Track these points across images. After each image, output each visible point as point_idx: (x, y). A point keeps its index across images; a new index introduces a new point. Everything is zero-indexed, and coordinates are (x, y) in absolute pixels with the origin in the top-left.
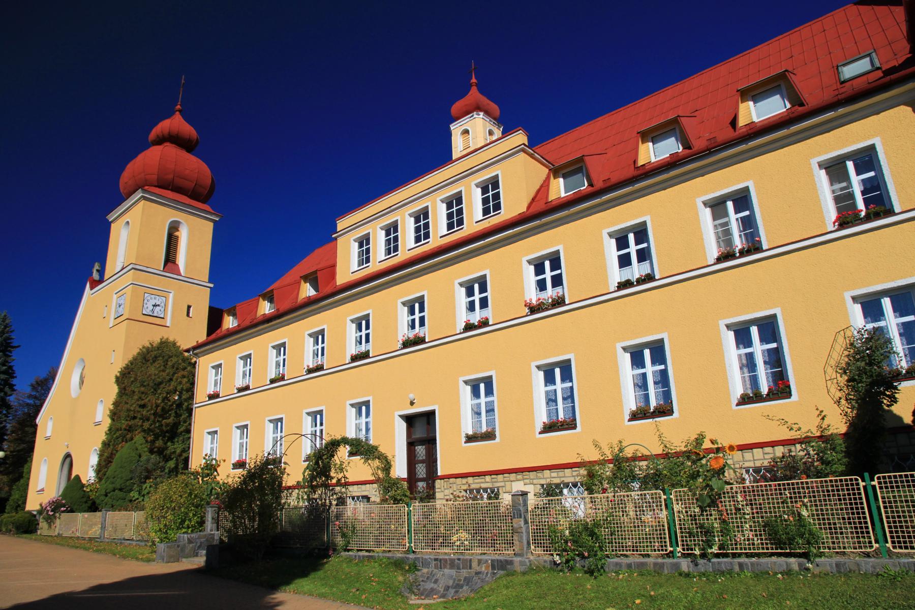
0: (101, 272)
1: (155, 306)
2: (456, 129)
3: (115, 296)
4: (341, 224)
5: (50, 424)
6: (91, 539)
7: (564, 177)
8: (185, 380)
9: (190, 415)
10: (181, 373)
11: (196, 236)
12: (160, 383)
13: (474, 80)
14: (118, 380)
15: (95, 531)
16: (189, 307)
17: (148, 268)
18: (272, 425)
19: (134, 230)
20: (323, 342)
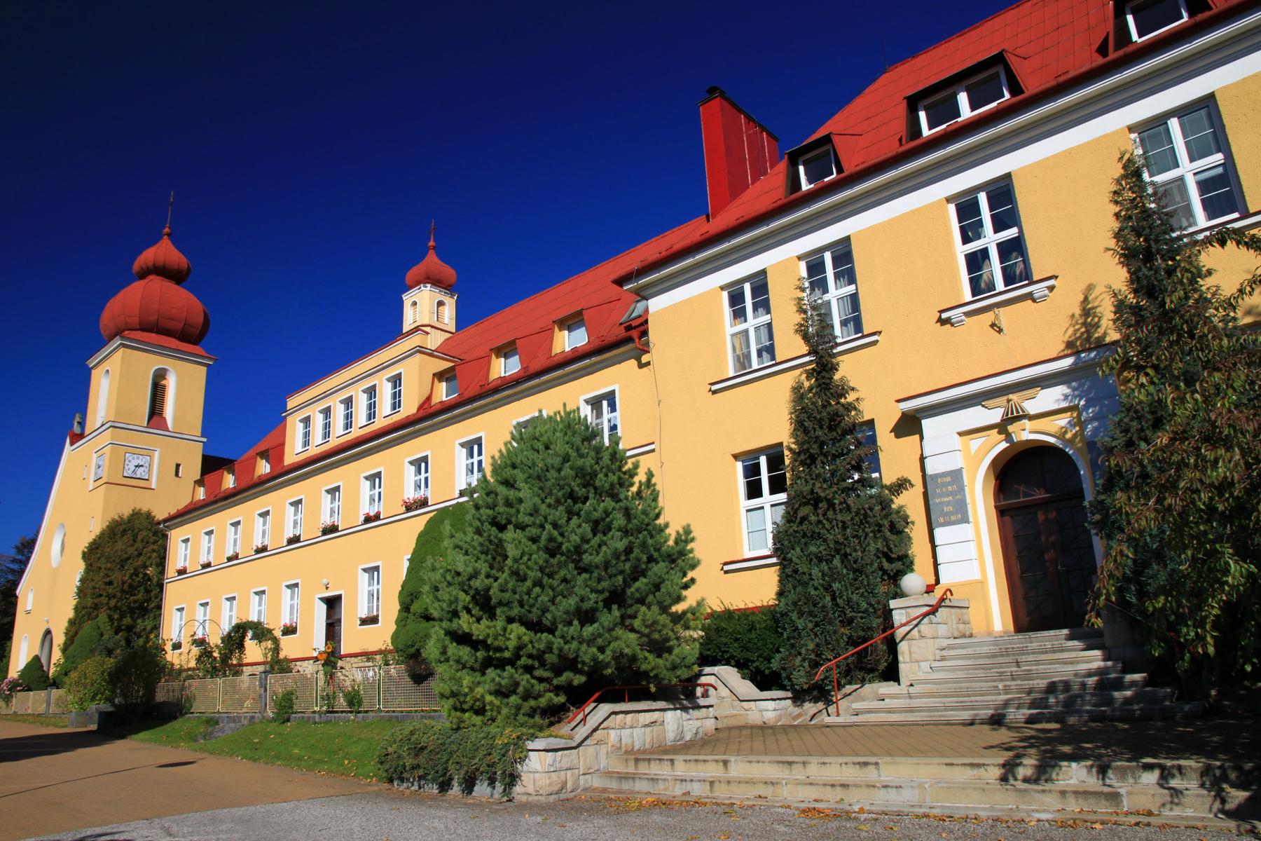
0: (82, 424)
2: (407, 299)
3: (95, 456)
4: (292, 403)
5: (31, 596)
6: (39, 715)
7: (447, 380)
8: (155, 555)
9: (162, 591)
10: (152, 547)
11: (186, 384)
12: (128, 559)
13: (432, 243)
14: (86, 556)
15: (42, 708)
16: (178, 466)
17: (130, 423)
18: (366, 575)
19: (115, 380)
20: (426, 471)
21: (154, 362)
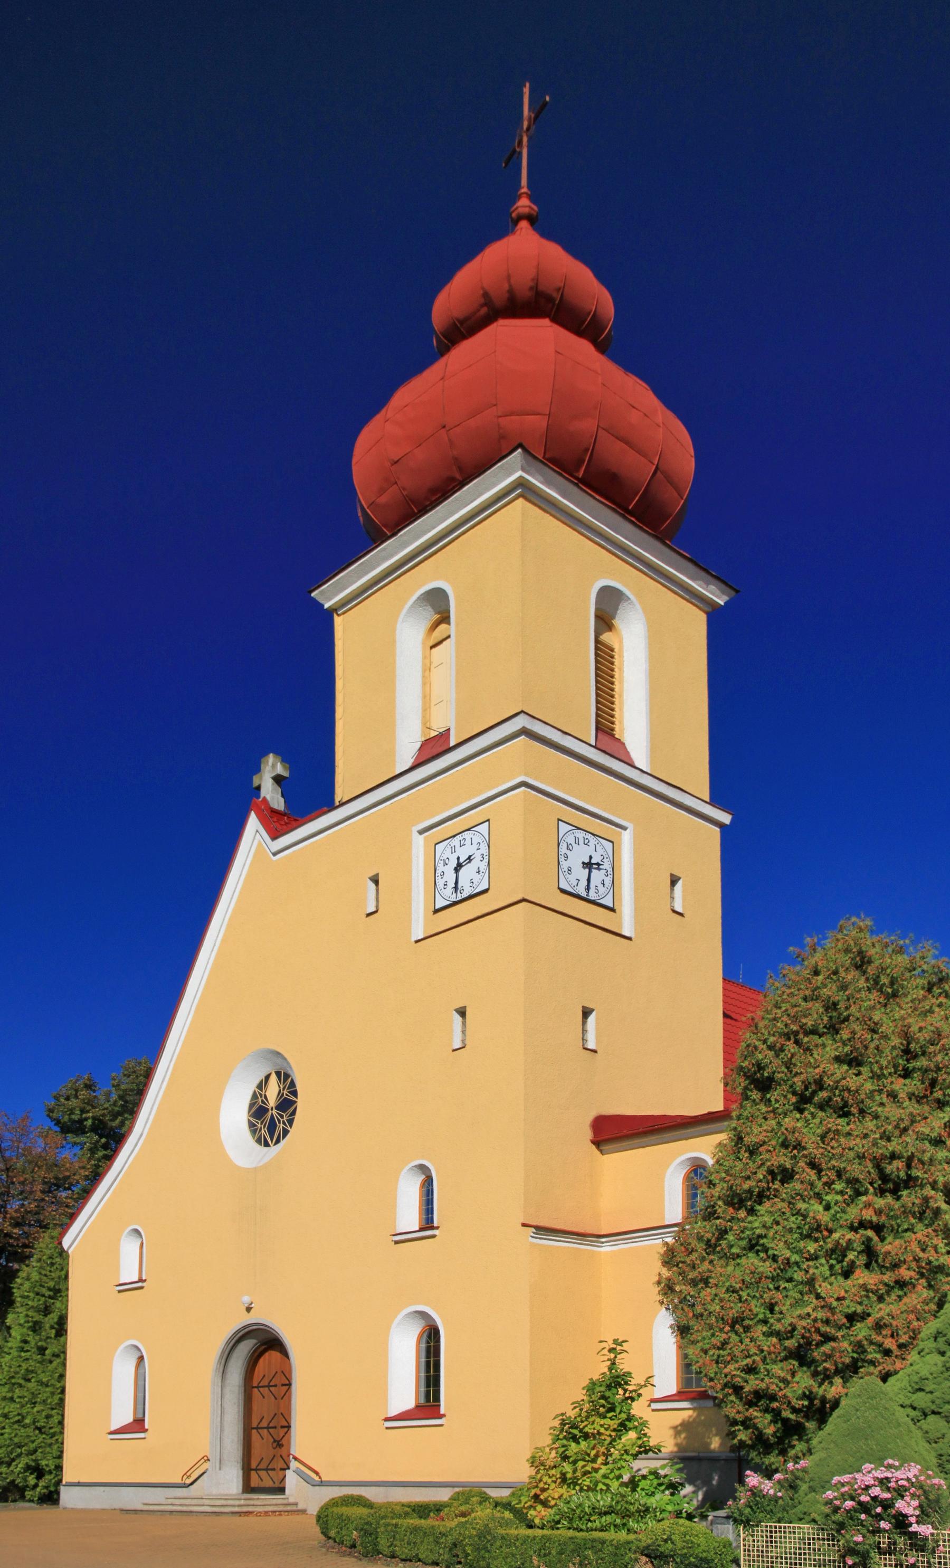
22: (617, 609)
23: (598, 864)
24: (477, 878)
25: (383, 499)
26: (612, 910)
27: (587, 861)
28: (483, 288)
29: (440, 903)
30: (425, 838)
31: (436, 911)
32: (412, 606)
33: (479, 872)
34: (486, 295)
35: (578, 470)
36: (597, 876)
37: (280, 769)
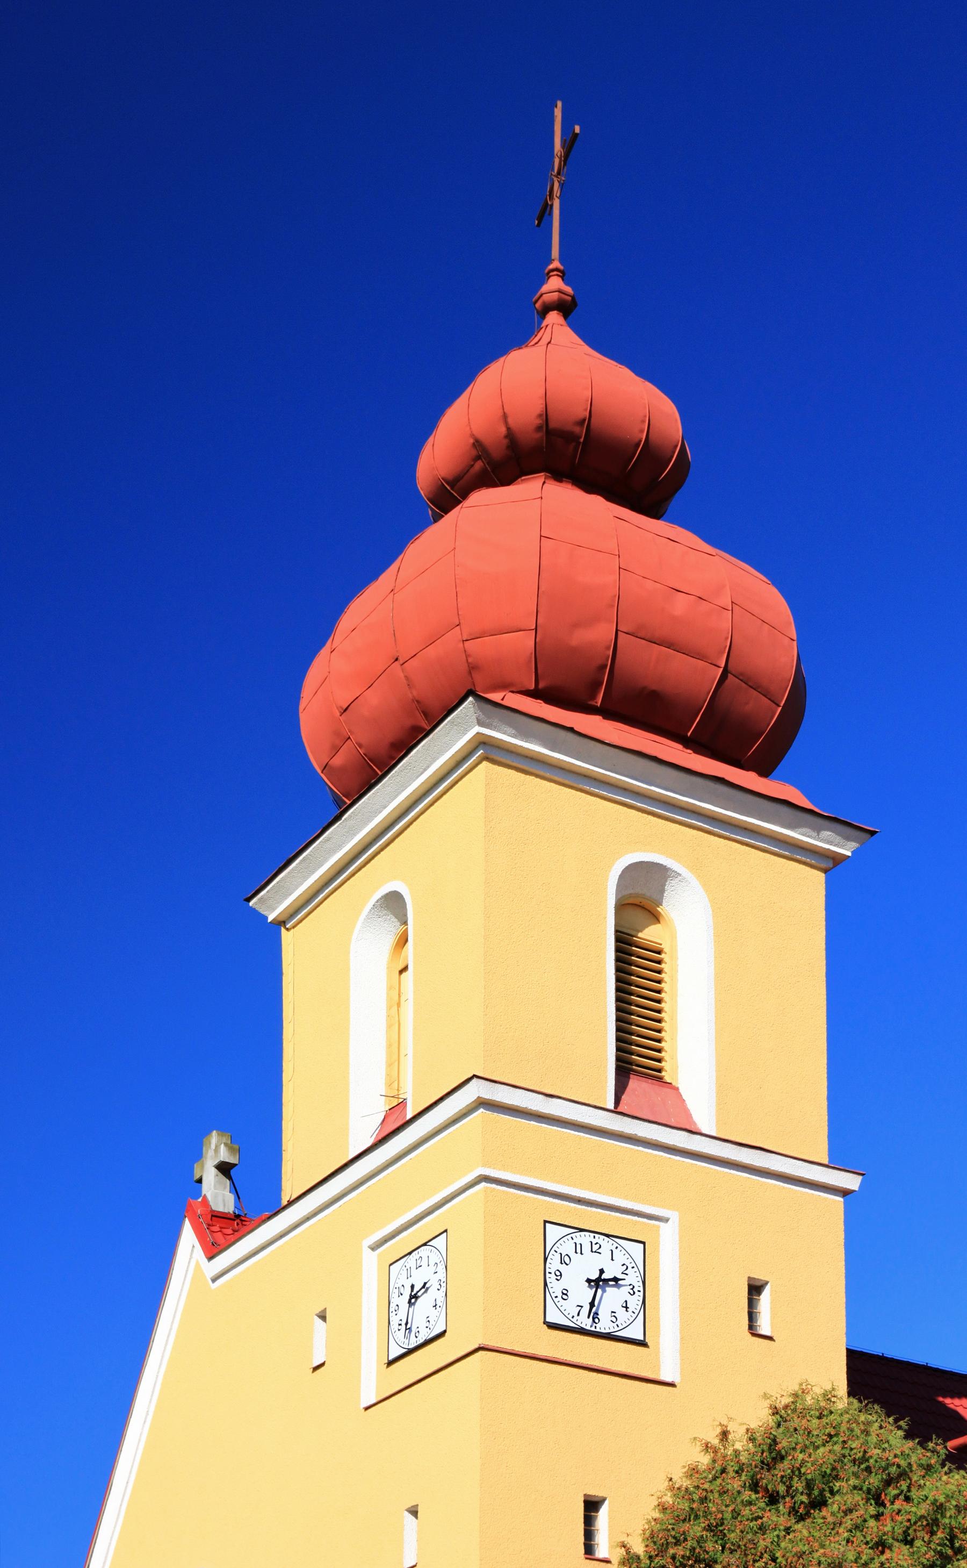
1: (598, 1283)
3: (371, 1262)
21: (624, 836)
22: (662, 891)
23: (616, 1280)
24: (433, 1313)
25: (337, 761)
26: (642, 1344)
27: (594, 1276)
28: (472, 435)
29: (394, 1353)
30: (379, 1256)
31: (390, 1363)
32: (368, 917)
33: (627, 1308)
34: (477, 444)
35: (593, 696)
36: (611, 1299)
37: (224, 1155)
